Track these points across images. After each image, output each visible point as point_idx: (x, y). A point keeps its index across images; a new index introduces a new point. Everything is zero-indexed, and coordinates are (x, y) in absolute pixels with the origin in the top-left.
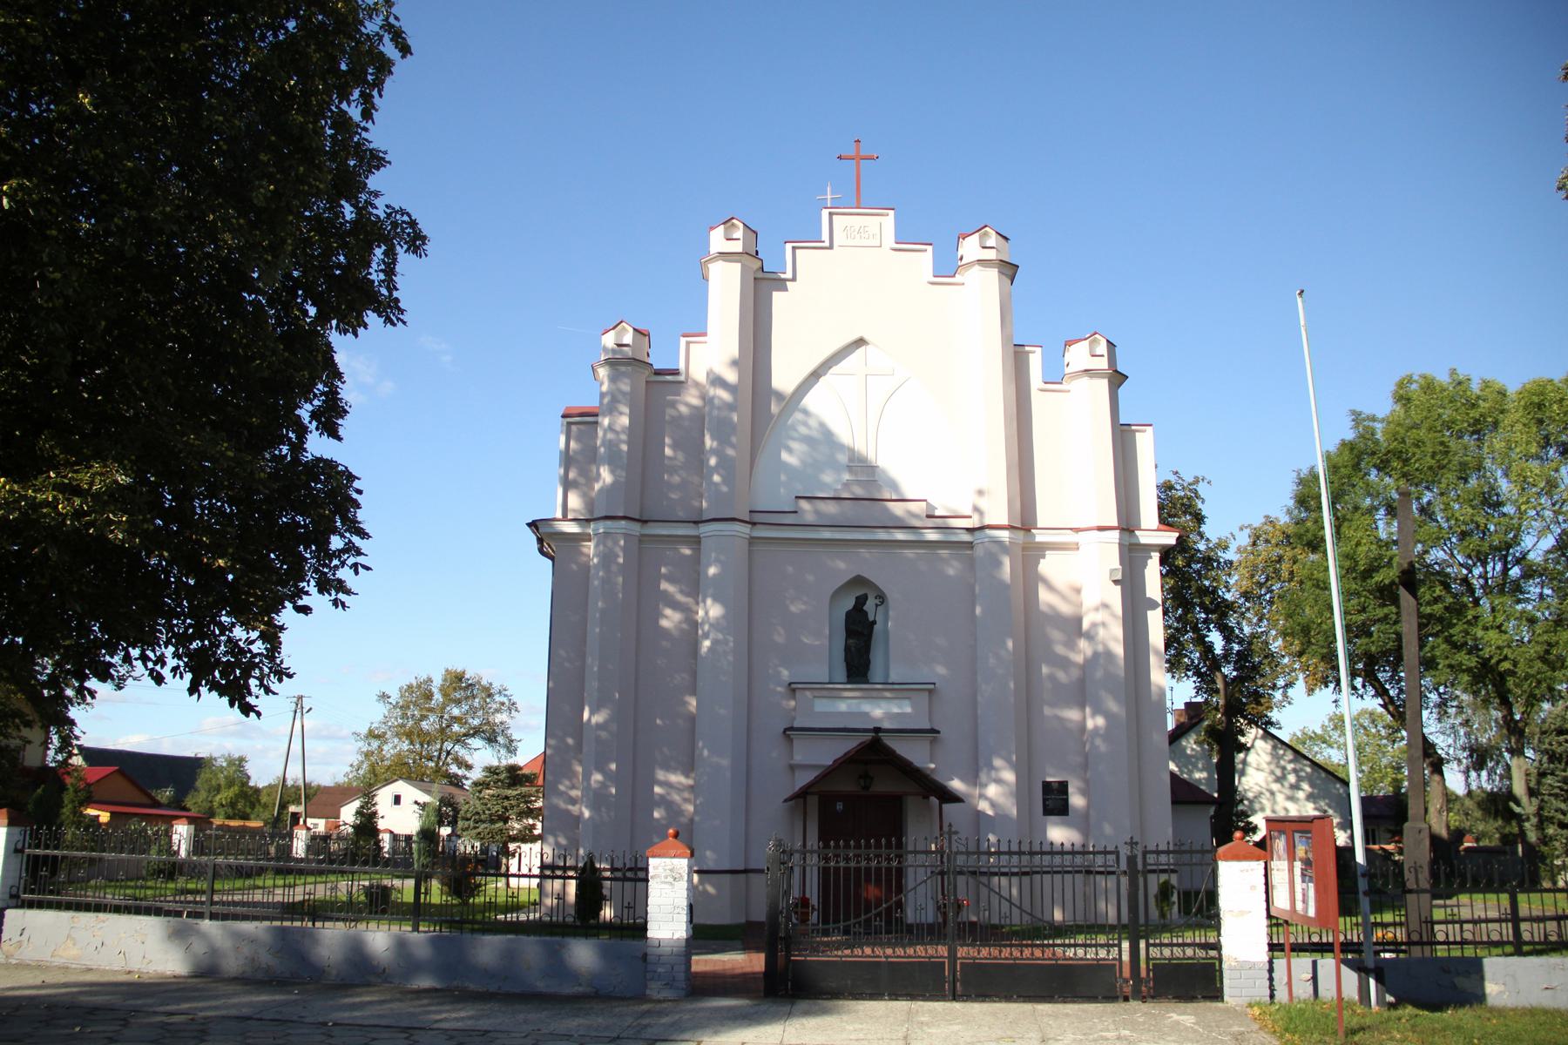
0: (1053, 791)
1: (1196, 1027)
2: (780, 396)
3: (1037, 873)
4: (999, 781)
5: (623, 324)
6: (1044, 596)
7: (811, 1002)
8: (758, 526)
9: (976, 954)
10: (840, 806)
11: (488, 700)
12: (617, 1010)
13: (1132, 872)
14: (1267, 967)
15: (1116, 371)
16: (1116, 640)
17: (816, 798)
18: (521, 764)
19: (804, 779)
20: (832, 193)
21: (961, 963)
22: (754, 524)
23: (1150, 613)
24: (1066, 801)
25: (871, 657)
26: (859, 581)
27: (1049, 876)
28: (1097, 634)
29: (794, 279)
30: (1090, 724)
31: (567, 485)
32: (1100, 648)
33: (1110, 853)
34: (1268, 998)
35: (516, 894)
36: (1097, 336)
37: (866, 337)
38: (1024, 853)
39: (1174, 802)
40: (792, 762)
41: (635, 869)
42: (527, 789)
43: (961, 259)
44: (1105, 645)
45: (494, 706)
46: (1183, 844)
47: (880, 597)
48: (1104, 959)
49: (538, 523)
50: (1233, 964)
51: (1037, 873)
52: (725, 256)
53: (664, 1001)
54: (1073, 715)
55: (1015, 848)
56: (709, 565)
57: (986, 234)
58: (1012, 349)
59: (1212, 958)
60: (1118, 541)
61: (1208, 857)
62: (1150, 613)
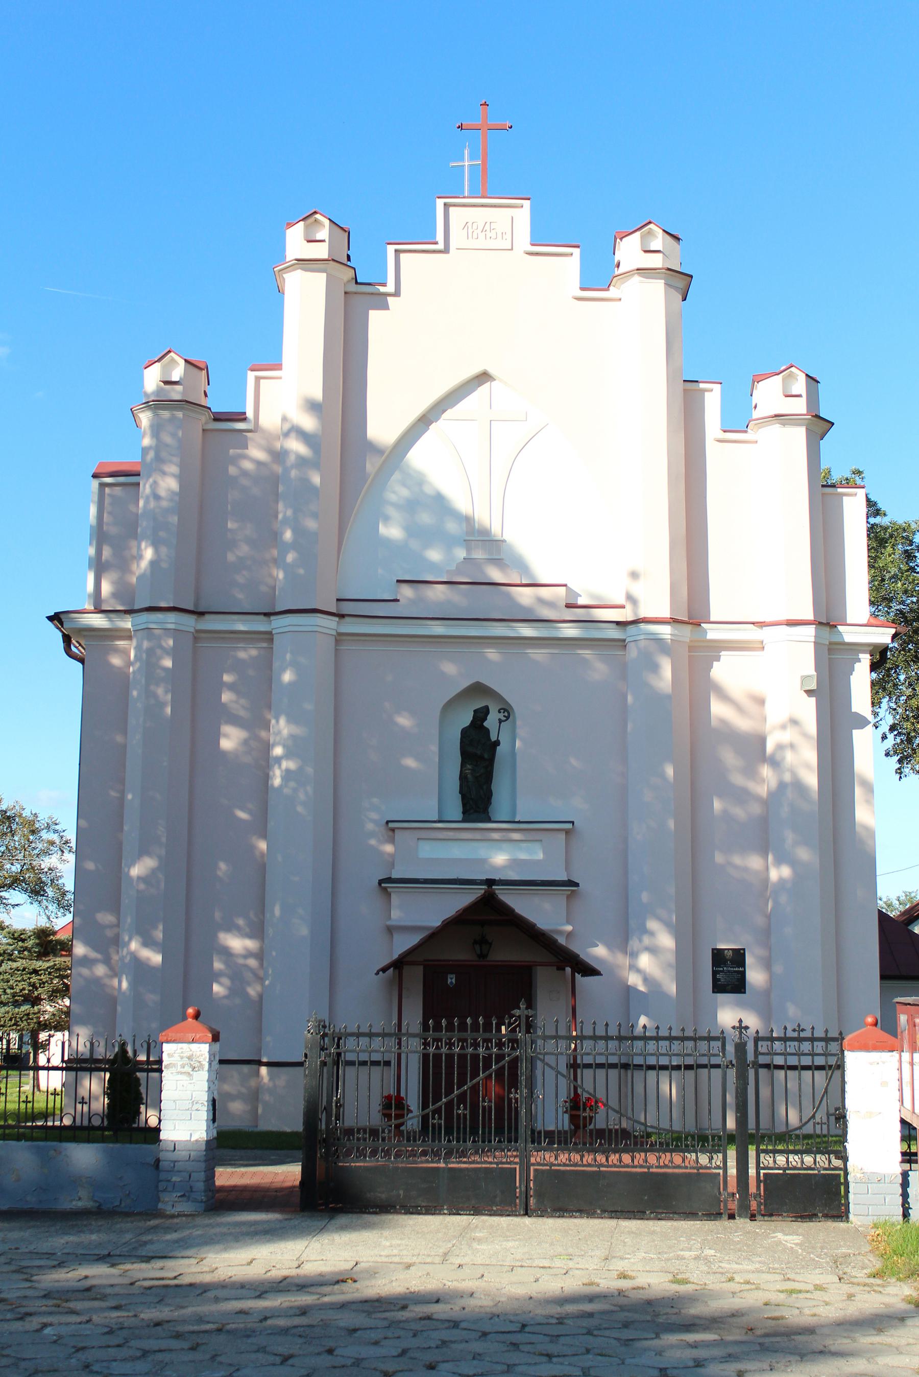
0: (726, 960)
1: (797, 1248)
2: (373, 448)
3: (705, 1066)
4: (653, 950)
5: (172, 354)
6: (718, 709)
7: (355, 1216)
8: (347, 619)
9: (552, 1159)
10: (452, 980)
11: (31, 837)
12: (118, 1226)
13: (741, 1064)
14: (900, 1180)
15: (817, 416)
16: (808, 766)
17: (419, 970)
18: (57, 928)
19: (404, 943)
20: (471, 159)
21: (536, 1170)
22: (342, 616)
23: (856, 733)
24: (743, 974)
25: (493, 787)
26: (478, 689)
27: (810, 1072)
28: (784, 758)
29: (397, 293)
30: (774, 874)
31: (99, 567)
32: (787, 777)
33: (716, 1039)
34: (901, 1218)
35: (30, 1099)
36: (793, 369)
37: (492, 371)
38: (612, 1038)
39: (883, 977)
40: (389, 923)
41: (820, 1125)
42: (63, 959)
43: (618, 265)
44: (794, 774)
45: (40, 846)
46: (803, 1030)
47: (505, 710)
48: (706, 1168)
49: (62, 616)
50: (859, 1175)
51: (705, 1066)
52: (304, 263)
53: (179, 1216)
54: (755, 862)
55: (600, 1032)
56: (284, 670)
57: (650, 232)
58: (681, 385)
59: (836, 1168)
60: (813, 639)
61: (833, 1047)
62: (856, 733)
